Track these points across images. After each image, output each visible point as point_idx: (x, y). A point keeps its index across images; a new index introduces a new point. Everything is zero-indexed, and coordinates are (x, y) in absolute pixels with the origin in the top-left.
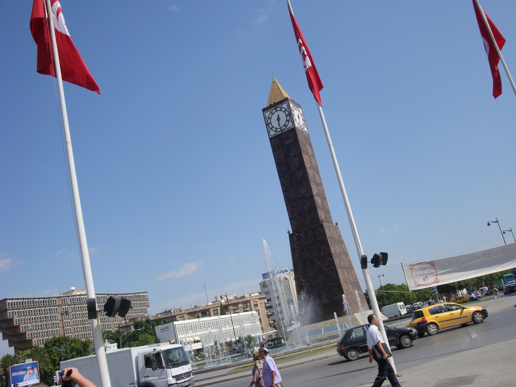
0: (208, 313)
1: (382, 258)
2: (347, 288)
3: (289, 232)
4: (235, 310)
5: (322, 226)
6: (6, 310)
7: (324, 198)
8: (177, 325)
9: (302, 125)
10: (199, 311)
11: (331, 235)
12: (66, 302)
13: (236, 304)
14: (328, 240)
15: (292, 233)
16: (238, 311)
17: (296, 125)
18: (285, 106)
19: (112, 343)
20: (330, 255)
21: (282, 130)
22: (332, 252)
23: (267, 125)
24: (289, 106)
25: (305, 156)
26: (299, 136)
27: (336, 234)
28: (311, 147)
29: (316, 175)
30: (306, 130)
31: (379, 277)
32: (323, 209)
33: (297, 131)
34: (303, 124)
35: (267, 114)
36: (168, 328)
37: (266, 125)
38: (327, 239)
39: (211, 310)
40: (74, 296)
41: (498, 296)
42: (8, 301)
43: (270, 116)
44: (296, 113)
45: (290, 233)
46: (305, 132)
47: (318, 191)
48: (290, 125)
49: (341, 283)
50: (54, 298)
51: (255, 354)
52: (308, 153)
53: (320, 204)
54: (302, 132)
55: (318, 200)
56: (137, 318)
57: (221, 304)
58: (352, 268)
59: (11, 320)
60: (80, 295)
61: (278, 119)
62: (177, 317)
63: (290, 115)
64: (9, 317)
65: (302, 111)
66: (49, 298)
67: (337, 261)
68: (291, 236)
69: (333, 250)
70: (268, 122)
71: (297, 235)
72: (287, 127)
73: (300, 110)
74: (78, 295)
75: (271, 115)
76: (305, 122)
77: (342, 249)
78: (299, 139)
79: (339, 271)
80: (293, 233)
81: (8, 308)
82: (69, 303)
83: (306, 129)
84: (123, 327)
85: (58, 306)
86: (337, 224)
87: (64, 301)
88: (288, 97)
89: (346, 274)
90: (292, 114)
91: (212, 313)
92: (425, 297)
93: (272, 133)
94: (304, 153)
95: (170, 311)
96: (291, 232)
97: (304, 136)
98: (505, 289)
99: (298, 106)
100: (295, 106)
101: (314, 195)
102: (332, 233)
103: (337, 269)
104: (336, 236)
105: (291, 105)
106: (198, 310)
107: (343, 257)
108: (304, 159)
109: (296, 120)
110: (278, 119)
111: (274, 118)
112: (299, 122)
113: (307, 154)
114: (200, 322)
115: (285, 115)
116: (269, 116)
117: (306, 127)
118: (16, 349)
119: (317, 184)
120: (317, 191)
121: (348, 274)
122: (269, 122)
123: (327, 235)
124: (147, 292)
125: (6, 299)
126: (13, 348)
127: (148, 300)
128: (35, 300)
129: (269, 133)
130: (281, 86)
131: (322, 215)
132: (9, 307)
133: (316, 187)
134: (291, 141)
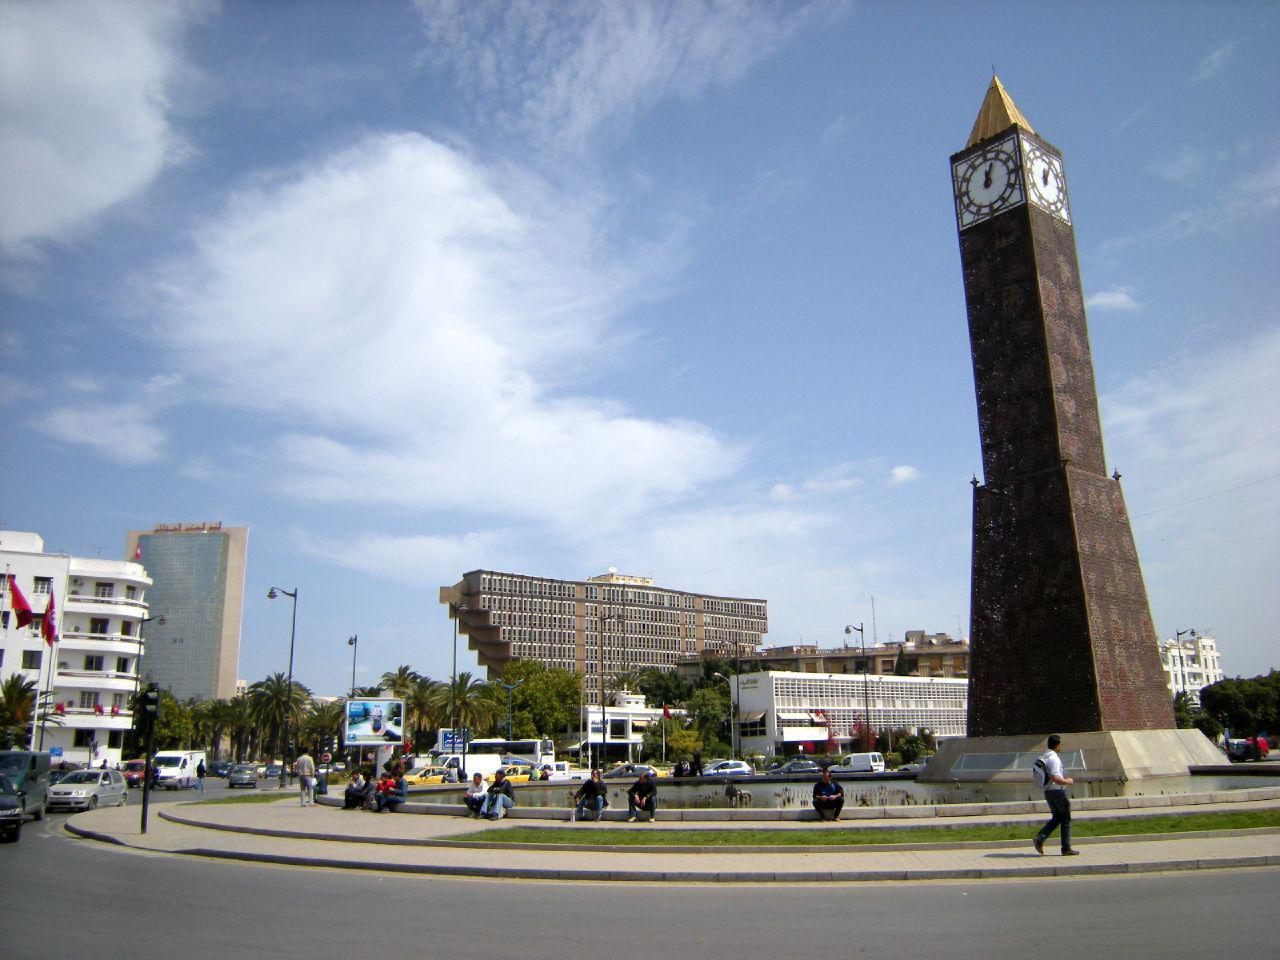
0: (870, 666)
1: (791, 657)
2: (1107, 657)
3: (975, 482)
4: (932, 669)
5: (1062, 476)
6: (478, 593)
7: (1088, 404)
8: (776, 679)
9: (1051, 201)
10: (851, 658)
11: (1087, 504)
12: (594, 595)
13: (941, 656)
14: (1074, 515)
15: (983, 484)
16: (942, 672)
17: (1033, 198)
18: (1008, 147)
19: (635, 693)
20: (1073, 555)
21: (993, 211)
22: (1079, 550)
23: (958, 196)
24: (1018, 148)
25: (1043, 283)
26: (1034, 228)
27: (1107, 503)
28: (1073, 263)
29: (1074, 337)
30: (1064, 214)
31: (1178, 634)
32: (1077, 431)
33: (1032, 214)
34: (1059, 200)
35: (962, 168)
36: (755, 682)
37: (956, 197)
38: (1071, 510)
39: (879, 661)
40: (611, 585)
41: (122, 771)
42: (484, 576)
43: (1009, 190)
44: (1036, 167)
45: (978, 485)
46: (1061, 221)
47: (1072, 381)
48: (1015, 198)
49: (1091, 638)
50: (571, 583)
51: (1144, 776)
52: (1058, 276)
53: (1070, 415)
54: (1049, 218)
55: (1065, 406)
56: (718, 651)
57: (901, 652)
58: (1144, 604)
59: (486, 614)
60: (624, 586)
61: (988, 183)
62: (803, 665)
63: (1018, 170)
64: (481, 606)
65: (1062, 166)
66: (562, 582)
67: (1089, 578)
68: (978, 493)
69: (1082, 544)
70: (960, 189)
71: (994, 493)
72: (1007, 204)
73: (1056, 164)
74: (619, 586)
75: (971, 170)
76: (1065, 194)
77: (1120, 545)
78: (1034, 236)
79: (1093, 608)
80: (986, 485)
81: (481, 589)
82: (600, 598)
83: (1064, 214)
84: (685, 665)
85: (578, 600)
86: (1117, 477)
87: (592, 592)
88: (1023, 123)
89: (1115, 617)
90: (1025, 168)
91: (880, 666)
92: (576, 697)
93: (968, 218)
94: (1042, 275)
95: (790, 649)
96: (982, 482)
97: (1055, 231)
98: (420, 718)
99: (1049, 150)
100: (1038, 149)
101: (1054, 389)
102: (1092, 497)
103: (1087, 598)
104: (1106, 507)
105: (1026, 146)
106: (849, 654)
107: (1118, 569)
108: (1041, 289)
109: (1034, 185)
110: (988, 183)
111: (979, 177)
112: (1044, 191)
113: (1056, 278)
114: (933, 684)
115: (1006, 172)
116: (1012, 192)
117: (1068, 209)
118: (491, 671)
119: (1069, 360)
120: (1068, 379)
121: (1124, 617)
122: (964, 189)
123: (1074, 501)
124: (765, 601)
125: (480, 572)
126: (485, 668)
127: (766, 619)
128: (535, 582)
129: (959, 216)
130: (1010, 99)
131: (1069, 445)
132: (484, 588)
133: (1065, 368)
134: (1011, 240)
